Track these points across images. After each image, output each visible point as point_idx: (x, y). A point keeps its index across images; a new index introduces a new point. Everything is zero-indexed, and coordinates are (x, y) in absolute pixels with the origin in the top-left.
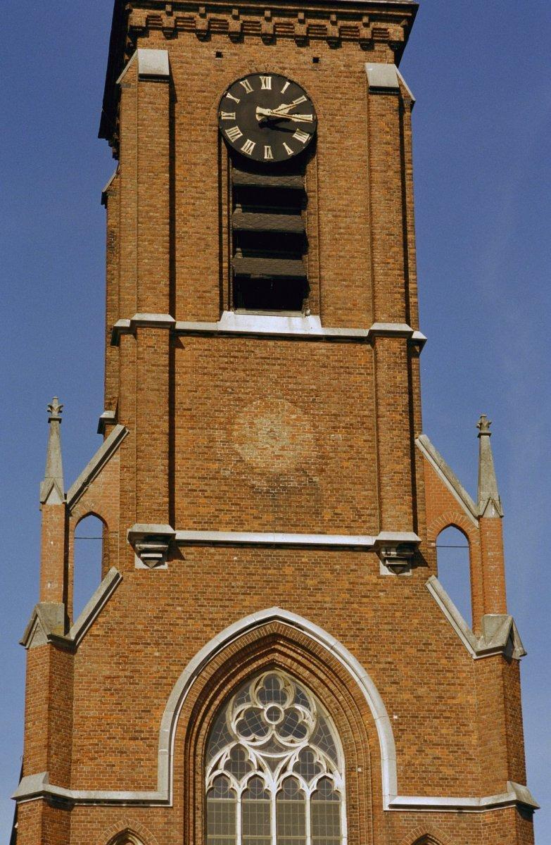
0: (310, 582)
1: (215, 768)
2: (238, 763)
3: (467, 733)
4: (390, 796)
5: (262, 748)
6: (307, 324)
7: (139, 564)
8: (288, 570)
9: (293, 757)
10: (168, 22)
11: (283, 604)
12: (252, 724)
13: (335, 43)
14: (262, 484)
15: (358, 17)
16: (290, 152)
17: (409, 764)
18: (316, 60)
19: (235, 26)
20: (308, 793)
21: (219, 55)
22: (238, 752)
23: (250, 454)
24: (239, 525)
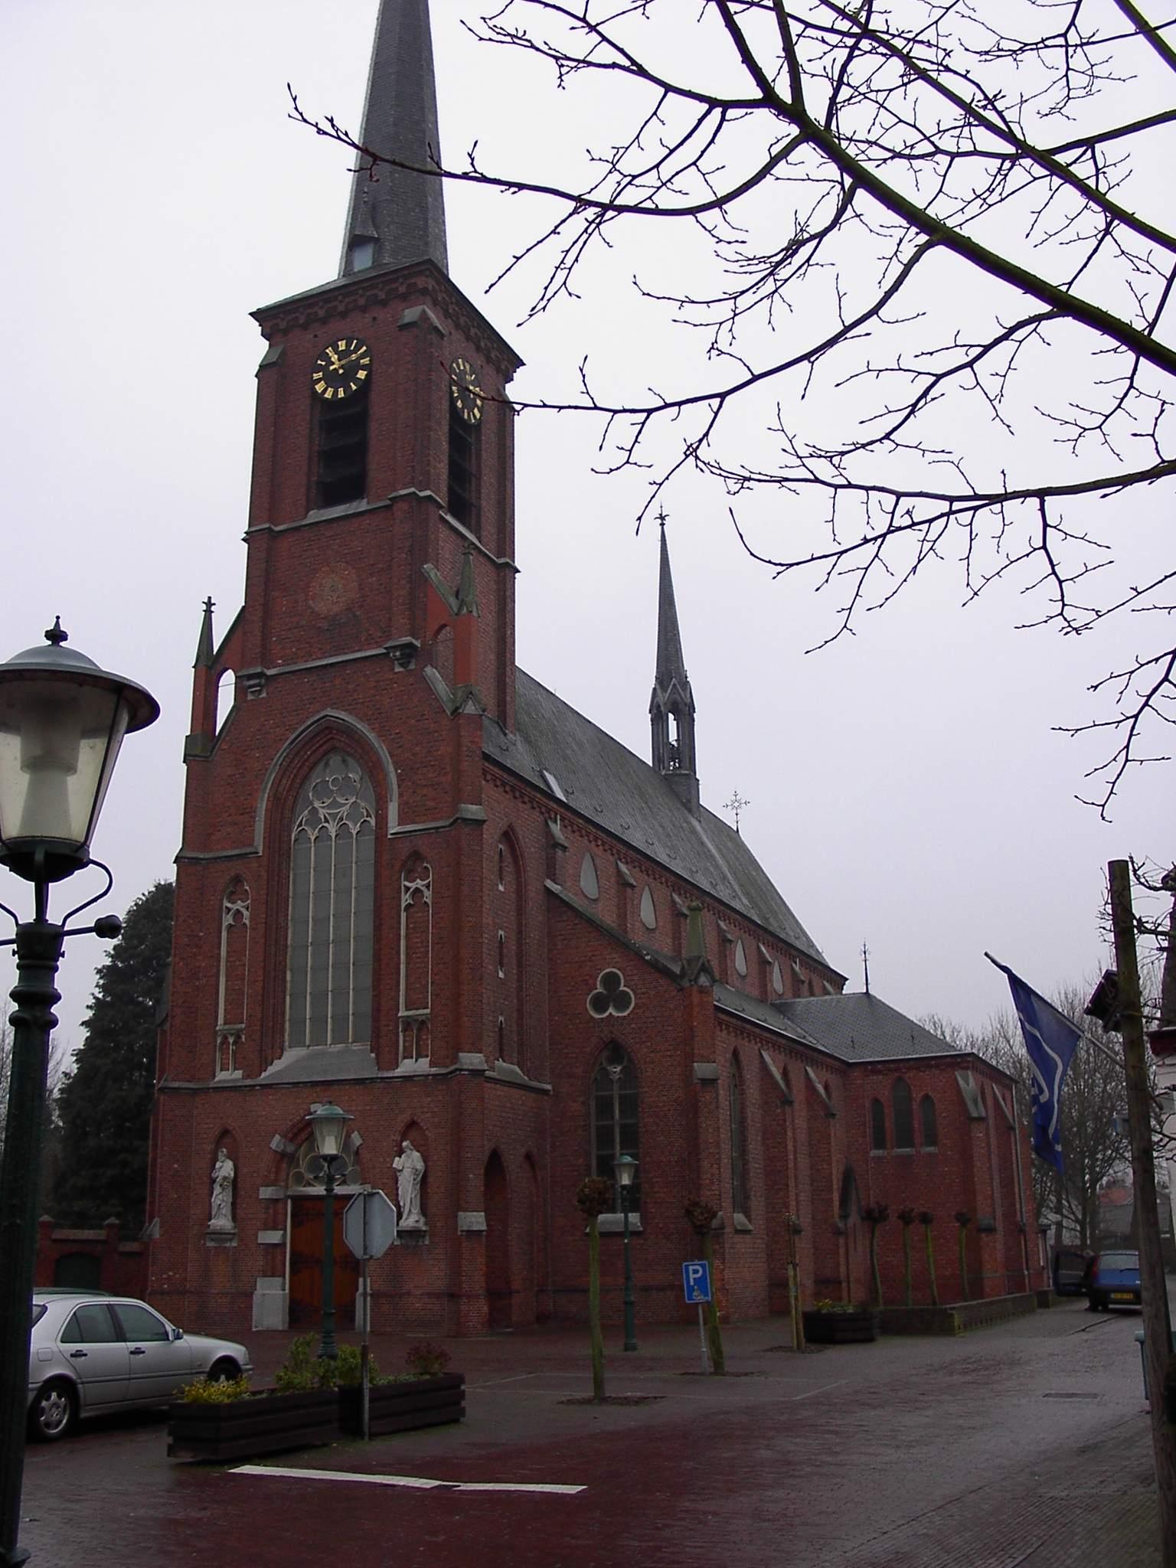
0: (351, 687)
1: (300, 825)
2: (314, 819)
3: (446, 774)
4: (393, 828)
5: (328, 807)
6: (362, 505)
7: (250, 697)
8: (338, 681)
9: (344, 811)
10: (283, 325)
11: (334, 706)
12: (322, 791)
13: (324, 321)
14: (325, 625)
15: (395, 280)
16: (354, 387)
17: (407, 803)
18: (375, 319)
19: (321, 313)
20: (354, 833)
21: (375, 319)
22: (315, 811)
23: (321, 607)
24: (310, 656)
